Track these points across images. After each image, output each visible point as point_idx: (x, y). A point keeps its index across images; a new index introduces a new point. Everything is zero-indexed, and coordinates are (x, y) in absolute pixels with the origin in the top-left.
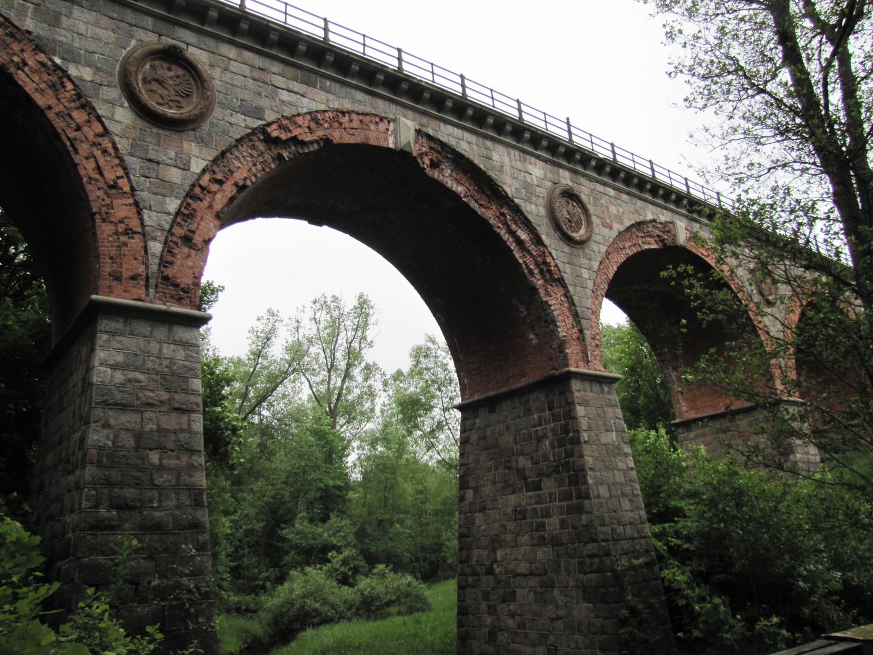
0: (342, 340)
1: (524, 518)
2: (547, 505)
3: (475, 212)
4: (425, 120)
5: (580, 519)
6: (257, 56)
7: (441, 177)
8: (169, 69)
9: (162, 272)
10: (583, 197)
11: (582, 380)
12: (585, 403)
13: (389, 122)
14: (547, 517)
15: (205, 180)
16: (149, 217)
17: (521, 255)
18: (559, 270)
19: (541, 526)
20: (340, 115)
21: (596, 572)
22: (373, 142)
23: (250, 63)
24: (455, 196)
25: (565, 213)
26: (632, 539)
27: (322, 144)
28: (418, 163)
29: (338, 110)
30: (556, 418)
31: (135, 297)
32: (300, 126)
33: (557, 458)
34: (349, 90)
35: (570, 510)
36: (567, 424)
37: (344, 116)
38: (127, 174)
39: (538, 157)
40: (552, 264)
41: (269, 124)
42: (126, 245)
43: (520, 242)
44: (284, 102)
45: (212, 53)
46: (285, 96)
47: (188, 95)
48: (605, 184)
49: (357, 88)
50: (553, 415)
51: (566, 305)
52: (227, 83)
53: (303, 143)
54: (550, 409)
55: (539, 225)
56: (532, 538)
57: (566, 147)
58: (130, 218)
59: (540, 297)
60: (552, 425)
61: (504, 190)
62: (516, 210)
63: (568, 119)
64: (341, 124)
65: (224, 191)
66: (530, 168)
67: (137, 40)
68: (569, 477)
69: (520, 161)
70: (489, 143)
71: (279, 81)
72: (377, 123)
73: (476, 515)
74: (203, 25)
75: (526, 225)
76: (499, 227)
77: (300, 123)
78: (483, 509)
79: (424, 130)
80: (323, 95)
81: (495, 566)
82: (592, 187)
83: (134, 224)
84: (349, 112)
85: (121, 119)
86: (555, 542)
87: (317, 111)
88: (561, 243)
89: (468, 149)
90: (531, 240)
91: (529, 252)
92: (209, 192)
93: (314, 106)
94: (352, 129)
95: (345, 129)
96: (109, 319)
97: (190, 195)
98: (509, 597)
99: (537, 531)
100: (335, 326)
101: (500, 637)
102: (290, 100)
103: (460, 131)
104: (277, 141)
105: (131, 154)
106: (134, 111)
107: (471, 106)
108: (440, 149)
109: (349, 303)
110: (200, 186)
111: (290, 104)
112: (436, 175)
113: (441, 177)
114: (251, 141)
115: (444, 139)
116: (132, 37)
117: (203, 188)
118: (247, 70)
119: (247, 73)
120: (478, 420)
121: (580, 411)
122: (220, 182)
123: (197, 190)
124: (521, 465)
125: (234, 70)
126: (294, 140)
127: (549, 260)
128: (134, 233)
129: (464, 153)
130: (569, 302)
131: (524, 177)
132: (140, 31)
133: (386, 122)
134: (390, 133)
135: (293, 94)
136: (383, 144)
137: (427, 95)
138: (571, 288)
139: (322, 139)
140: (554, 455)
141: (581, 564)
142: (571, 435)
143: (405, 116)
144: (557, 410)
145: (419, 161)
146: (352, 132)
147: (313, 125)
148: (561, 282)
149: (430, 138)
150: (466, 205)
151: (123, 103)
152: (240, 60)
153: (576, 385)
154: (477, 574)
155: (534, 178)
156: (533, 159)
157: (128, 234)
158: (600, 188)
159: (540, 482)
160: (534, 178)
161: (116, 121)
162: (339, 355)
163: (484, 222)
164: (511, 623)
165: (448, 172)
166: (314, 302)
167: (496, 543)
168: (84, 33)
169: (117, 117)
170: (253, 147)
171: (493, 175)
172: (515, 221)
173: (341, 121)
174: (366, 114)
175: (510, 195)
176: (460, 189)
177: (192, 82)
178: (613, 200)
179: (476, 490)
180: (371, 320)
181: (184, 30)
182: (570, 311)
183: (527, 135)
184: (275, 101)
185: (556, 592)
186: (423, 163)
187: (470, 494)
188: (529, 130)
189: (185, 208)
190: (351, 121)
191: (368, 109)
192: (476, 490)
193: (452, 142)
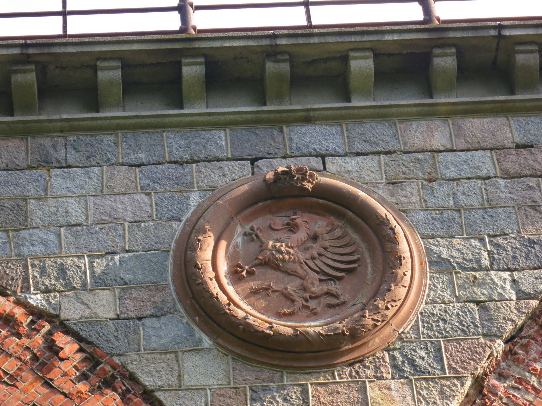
6: (501, 120)
8: (292, 227)
17: (76, 347)
23: (490, 142)
45: (386, 153)
52: (444, 209)
67: (201, 190)
74: (512, 93)
85: (203, 381)
116: (189, 187)
119: (487, 168)
125: (451, 173)
132: (207, 169)
151: (200, 341)
152: (464, 146)
161: (189, 389)
168: (82, 219)
169: (189, 380)
177: (355, 237)
181: (304, 129)
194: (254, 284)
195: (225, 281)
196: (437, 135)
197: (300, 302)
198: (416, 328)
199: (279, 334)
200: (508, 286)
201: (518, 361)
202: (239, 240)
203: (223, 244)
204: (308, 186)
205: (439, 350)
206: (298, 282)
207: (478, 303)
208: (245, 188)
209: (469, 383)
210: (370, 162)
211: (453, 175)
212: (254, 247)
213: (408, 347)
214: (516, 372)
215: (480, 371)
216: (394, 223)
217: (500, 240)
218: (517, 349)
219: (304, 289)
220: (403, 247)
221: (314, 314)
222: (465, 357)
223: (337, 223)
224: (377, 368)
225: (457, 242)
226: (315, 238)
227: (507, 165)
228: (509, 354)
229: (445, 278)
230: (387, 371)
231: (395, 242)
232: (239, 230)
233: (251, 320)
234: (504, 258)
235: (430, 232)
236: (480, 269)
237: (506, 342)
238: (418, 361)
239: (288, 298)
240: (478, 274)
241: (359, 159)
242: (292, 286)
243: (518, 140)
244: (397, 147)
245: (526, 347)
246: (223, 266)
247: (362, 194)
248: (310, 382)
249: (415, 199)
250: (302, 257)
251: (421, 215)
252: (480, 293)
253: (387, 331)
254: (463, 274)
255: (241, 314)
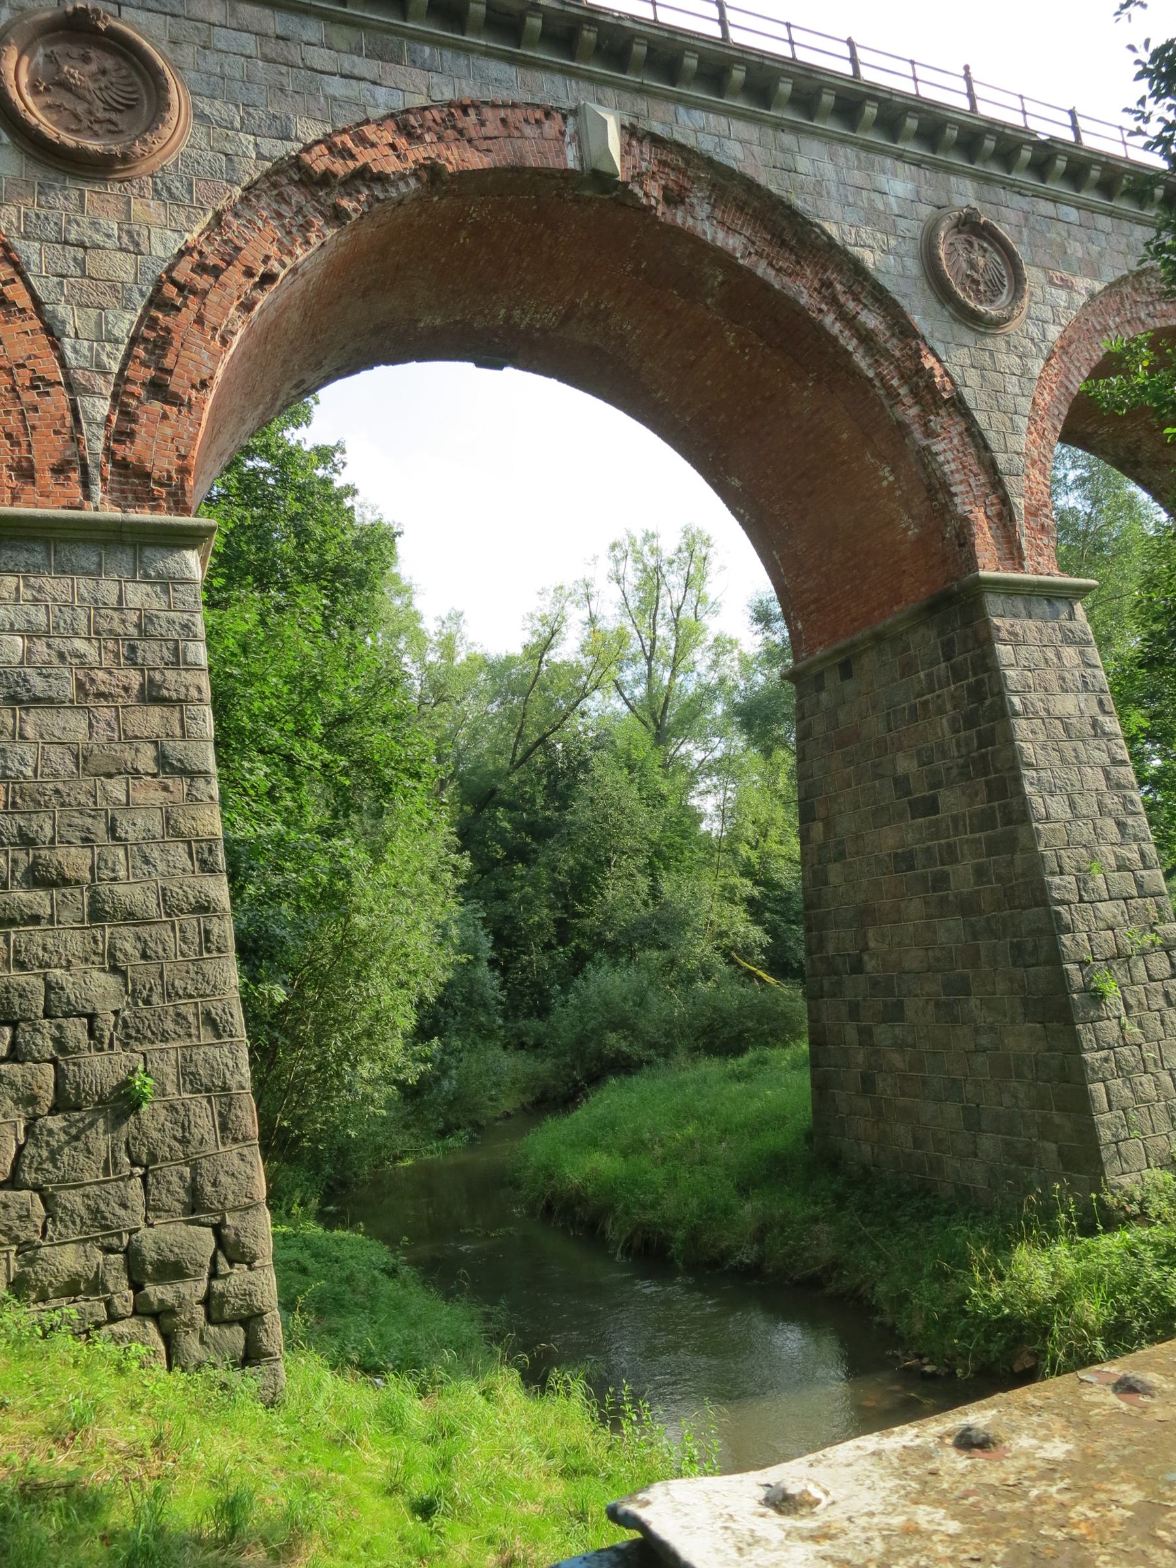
0: (665, 605)
1: (911, 867)
2: (951, 840)
3: (766, 286)
4: (642, 105)
5: (1011, 863)
6: (268, 12)
7: (690, 221)
8: (86, 59)
9: (113, 453)
10: (1003, 230)
11: (1009, 595)
12: (1016, 641)
13: (565, 118)
14: (951, 863)
15: (184, 271)
16: (76, 351)
18: (953, 383)
19: (941, 881)
20: (457, 113)
21: (1045, 963)
22: (532, 161)
23: (256, 28)
24: (724, 259)
25: (964, 265)
26: (1125, 899)
27: (425, 176)
28: (637, 199)
29: (450, 105)
30: (957, 674)
31: (65, 502)
32: (373, 145)
33: (964, 751)
34: (473, 59)
35: (993, 847)
36: (980, 683)
37: (465, 112)
38: (21, 274)
39: (899, 157)
40: (938, 371)
41: (307, 149)
42: (35, 409)
43: (866, 338)
44: (335, 99)
45: (173, 15)
46: (336, 87)
47: (129, 107)
48: (1055, 200)
49: (488, 53)
50: (953, 668)
51: (972, 450)
52: (211, 74)
53: (381, 179)
54: (948, 658)
55: (905, 296)
56: (926, 903)
57: (962, 126)
58: (36, 357)
59: (914, 442)
60: (952, 687)
61: (824, 232)
62: (857, 269)
63: (967, 68)
64: (461, 132)
65: (223, 286)
66: (882, 181)
67: (12, 8)
68: (988, 783)
69: (859, 168)
70: (788, 139)
71: (320, 58)
72: (538, 121)
73: (830, 866)
74: (405, 20)
75: (876, 300)
76: (820, 311)
77: (373, 138)
78: (841, 856)
79: (641, 125)
80: (418, 77)
81: (866, 958)
82: (1026, 207)
83: (49, 367)
84: (476, 105)
86: (967, 907)
87: (407, 111)
88: (956, 327)
89: (741, 156)
90: (890, 327)
91: (887, 354)
92: (194, 292)
93: (399, 102)
94: (486, 138)
95: (470, 141)
96: (13, 548)
97: (157, 301)
98: (895, 1013)
99: (935, 891)
100: (653, 580)
101: (880, 1085)
102: (350, 93)
103: (723, 120)
104: (327, 179)
105: (26, 237)
106: (23, 151)
107: (741, 61)
108: (681, 164)
109: (670, 544)
110: (174, 283)
111: (349, 102)
112: (679, 217)
113: (690, 221)
114: (275, 185)
115: (690, 142)
117: (181, 288)
118: (249, 44)
120: (824, 696)
121: (1004, 652)
122: (216, 272)
123: (170, 291)
124: (900, 771)
125: (221, 45)
126: (364, 175)
127: (929, 362)
128: (50, 384)
129: (734, 165)
130: (976, 446)
131: (870, 200)
133: (558, 117)
134: (567, 139)
135: (353, 82)
136: (553, 162)
137: (640, 50)
138: (980, 417)
139: (423, 166)
140: (958, 745)
141: (1018, 948)
142: (988, 702)
143: (599, 102)
144: (961, 658)
145: (637, 190)
146: (486, 144)
147: (402, 142)
148: (958, 406)
149: (657, 141)
150: (750, 273)
152: (235, 25)
153: (994, 604)
154: (836, 973)
155: (892, 200)
156: (889, 162)
157: (37, 387)
158: (1046, 207)
159: (934, 799)
160: (892, 200)
162: (663, 631)
163: (786, 304)
164: (897, 1059)
165: (703, 210)
166: (614, 547)
167: (865, 916)
170: (282, 199)
171: (798, 203)
172: (853, 293)
173: (460, 125)
174: (514, 106)
175: (839, 242)
176: (733, 243)
177: (137, 80)
178: (1075, 230)
179: (828, 823)
180: (713, 567)
182: (980, 462)
183: (871, 110)
184: (317, 100)
185: (974, 1002)
186: (646, 195)
187: (818, 828)
188: (874, 98)
189: (147, 327)
190: (482, 123)
191: (521, 96)
192: (828, 823)
193: (706, 144)
194: (49, 99)
195: (24, 91)
196: (215, 11)
197: (86, 123)
198: (176, 165)
199: (63, 144)
200: (251, 147)
201: (251, 207)
202: (40, 58)
203: (25, 59)
204: (102, 27)
205: (191, 185)
206: (86, 106)
207: (226, 155)
208: (48, 14)
209: (210, 214)
210: (158, 20)
211: (224, 48)
212: (52, 68)
213: (167, 178)
214: (247, 214)
215: (219, 208)
216: (168, 74)
217: (251, 110)
218: (251, 197)
219: (90, 113)
220: (173, 96)
221: (96, 135)
222: (210, 194)
223: (124, 64)
224: (141, 188)
225: (218, 103)
226: (104, 72)
227: (267, 51)
228: (244, 199)
229: (204, 130)
230: (150, 193)
231: (167, 90)
232: (41, 51)
233: (42, 128)
234: (252, 123)
235: (197, 90)
236: (232, 129)
237: (244, 190)
238: (174, 190)
239: (76, 116)
240: (230, 133)
241: (150, 14)
242: (80, 108)
243: (278, 32)
244: (181, 12)
245: (258, 197)
246: (24, 79)
247: (146, 44)
248: (87, 188)
249: (190, 60)
250: (91, 86)
251: (193, 75)
252: (229, 148)
253: (152, 161)
254: (218, 130)
255: (34, 121)
